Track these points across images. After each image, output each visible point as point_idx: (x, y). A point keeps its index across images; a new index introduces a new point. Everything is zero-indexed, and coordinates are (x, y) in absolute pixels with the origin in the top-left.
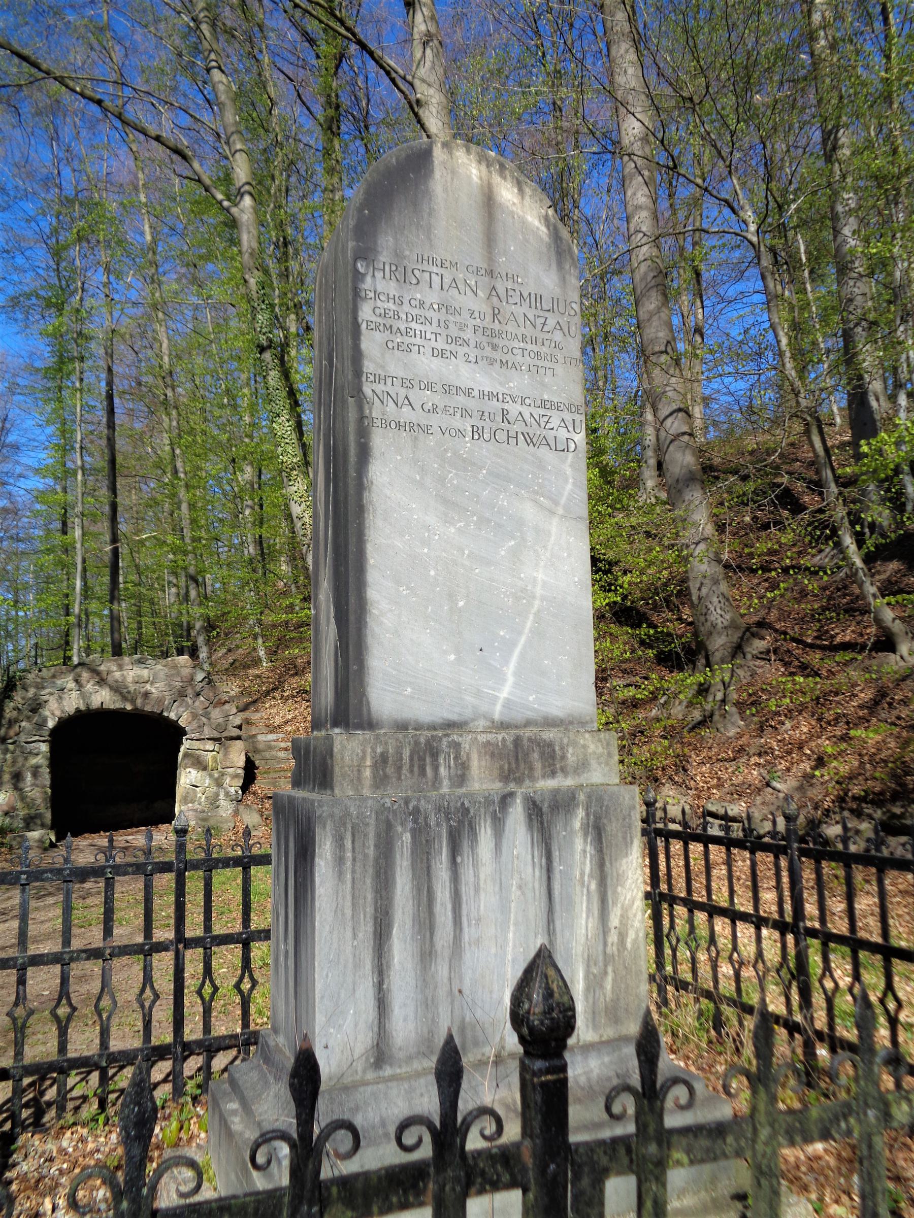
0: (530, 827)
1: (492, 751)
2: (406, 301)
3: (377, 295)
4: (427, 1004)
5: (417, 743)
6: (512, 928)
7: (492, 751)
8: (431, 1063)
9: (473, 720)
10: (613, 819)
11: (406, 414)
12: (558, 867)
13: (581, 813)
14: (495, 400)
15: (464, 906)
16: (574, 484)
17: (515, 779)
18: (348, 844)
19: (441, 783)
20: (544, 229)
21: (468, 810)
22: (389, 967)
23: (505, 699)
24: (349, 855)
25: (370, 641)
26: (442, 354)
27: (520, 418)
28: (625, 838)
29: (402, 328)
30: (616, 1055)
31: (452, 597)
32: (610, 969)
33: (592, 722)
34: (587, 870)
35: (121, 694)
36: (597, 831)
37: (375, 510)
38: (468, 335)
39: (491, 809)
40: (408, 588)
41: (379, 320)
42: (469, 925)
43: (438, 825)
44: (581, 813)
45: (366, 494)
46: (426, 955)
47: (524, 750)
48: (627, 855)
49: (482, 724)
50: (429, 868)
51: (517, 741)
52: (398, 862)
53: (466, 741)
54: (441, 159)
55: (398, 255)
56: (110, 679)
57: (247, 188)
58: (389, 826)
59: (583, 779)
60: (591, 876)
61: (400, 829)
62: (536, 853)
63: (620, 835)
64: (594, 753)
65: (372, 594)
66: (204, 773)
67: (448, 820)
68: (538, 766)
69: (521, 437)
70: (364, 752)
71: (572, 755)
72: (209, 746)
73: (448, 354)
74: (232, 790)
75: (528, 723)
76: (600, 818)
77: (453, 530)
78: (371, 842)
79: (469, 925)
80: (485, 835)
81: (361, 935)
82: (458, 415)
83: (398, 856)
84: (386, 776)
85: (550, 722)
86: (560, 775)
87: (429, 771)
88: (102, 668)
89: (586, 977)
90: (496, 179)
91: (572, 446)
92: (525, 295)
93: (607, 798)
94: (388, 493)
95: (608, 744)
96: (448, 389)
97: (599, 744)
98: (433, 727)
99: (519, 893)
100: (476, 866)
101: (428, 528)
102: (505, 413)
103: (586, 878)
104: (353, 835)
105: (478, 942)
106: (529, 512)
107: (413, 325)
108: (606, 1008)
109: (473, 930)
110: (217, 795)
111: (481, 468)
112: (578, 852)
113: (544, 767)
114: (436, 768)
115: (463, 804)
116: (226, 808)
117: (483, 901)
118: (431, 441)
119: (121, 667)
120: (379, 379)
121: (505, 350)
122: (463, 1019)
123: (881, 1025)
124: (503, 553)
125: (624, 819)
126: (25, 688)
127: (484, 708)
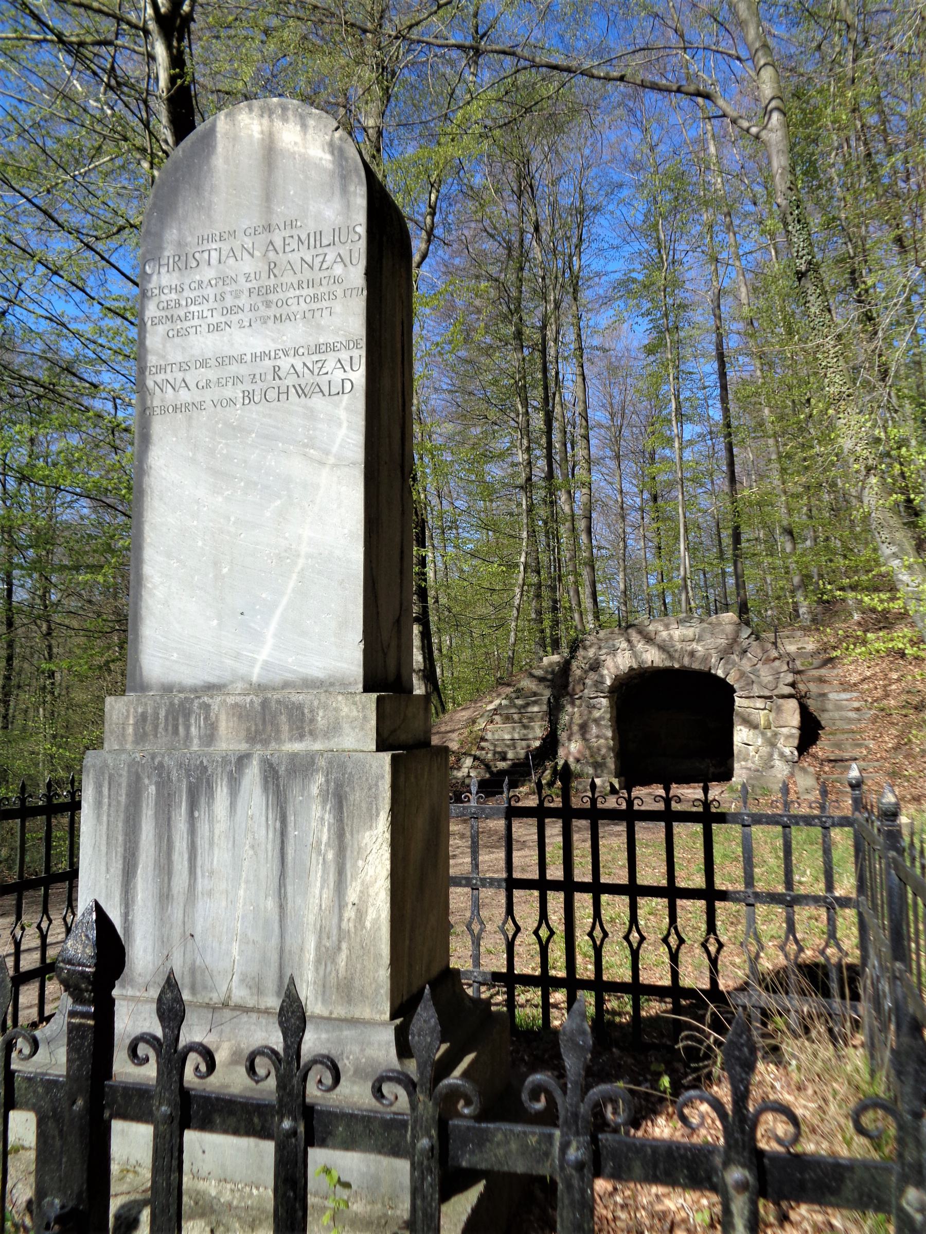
0: (266, 789)
1: (240, 712)
2: (186, 287)
3: (161, 289)
4: (163, 941)
5: (172, 704)
6: (243, 885)
7: (240, 712)
8: (154, 993)
9: (232, 682)
10: (357, 787)
11: (184, 396)
12: (292, 833)
13: (320, 779)
14: (267, 358)
15: (199, 858)
16: (349, 428)
17: (261, 741)
18: (105, 791)
19: (191, 742)
20: (328, 157)
21: (206, 768)
22: (133, 902)
23: (266, 662)
24: (106, 800)
25: (144, 612)
26: (217, 328)
27: (292, 371)
28: (369, 810)
29: (182, 314)
30: (335, 1034)
31: (216, 564)
32: (344, 946)
33: (356, 683)
34: (325, 838)
35: (668, 652)
36: (338, 798)
37: (152, 492)
38: (244, 300)
39: (228, 768)
40: (179, 561)
41: (163, 314)
42: (203, 876)
43: (179, 780)
44: (320, 779)
45: (146, 479)
46: (164, 897)
47: (274, 711)
48: (371, 827)
49: (240, 686)
50: (169, 819)
51: (265, 704)
52: (144, 811)
53: (215, 703)
54: (223, 131)
55: (180, 244)
56: (658, 639)
57: (773, 104)
58: (138, 778)
59: (333, 744)
60: (328, 844)
61: (146, 781)
62: (270, 816)
63: (364, 805)
64: (348, 716)
65: (149, 570)
66: (757, 732)
67: (189, 776)
68: (285, 728)
69: (292, 390)
70: (128, 711)
71: (323, 717)
72: (759, 703)
73: (223, 326)
74: (787, 751)
75: (286, 685)
76: (342, 786)
77: (220, 499)
78: (123, 792)
79: (203, 876)
80: (222, 793)
81: (112, 870)
82: (230, 384)
83: (144, 805)
84: (145, 734)
85: (309, 684)
86: (308, 738)
87: (181, 730)
88: (651, 628)
89: (318, 947)
90: (278, 124)
91: (348, 386)
92: (304, 237)
93: (350, 764)
94: (164, 474)
95: (364, 707)
96: (221, 361)
97: (353, 707)
98: (194, 690)
99: (251, 852)
100: (211, 821)
101: (197, 502)
102: (276, 370)
103: (323, 847)
104: (110, 784)
105: (210, 893)
106: (296, 467)
107: (193, 308)
108: (338, 984)
109: (206, 881)
110: (771, 755)
111: (250, 432)
112: (314, 819)
113: (291, 730)
114: (187, 728)
115: (202, 762)
116: (781, 769)
117: (218, 857)
118: (203, 417)
119: (667, 627)
120: (161, 369)
121: (280, 304)
122: (194, 961)
123: (755, 1100)
124: (268, 514)
125: (370, 789)
126: (585, 648)
127: (242, 669)
